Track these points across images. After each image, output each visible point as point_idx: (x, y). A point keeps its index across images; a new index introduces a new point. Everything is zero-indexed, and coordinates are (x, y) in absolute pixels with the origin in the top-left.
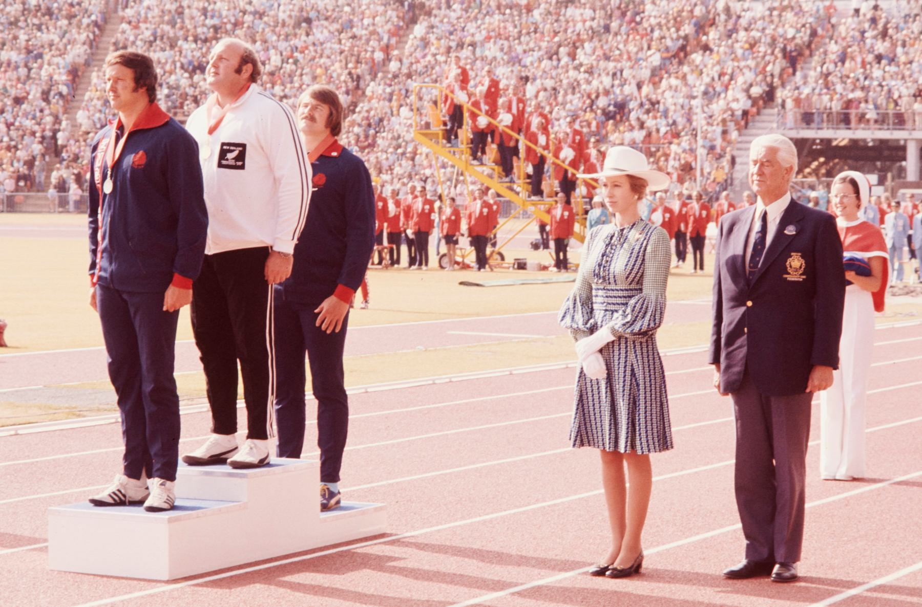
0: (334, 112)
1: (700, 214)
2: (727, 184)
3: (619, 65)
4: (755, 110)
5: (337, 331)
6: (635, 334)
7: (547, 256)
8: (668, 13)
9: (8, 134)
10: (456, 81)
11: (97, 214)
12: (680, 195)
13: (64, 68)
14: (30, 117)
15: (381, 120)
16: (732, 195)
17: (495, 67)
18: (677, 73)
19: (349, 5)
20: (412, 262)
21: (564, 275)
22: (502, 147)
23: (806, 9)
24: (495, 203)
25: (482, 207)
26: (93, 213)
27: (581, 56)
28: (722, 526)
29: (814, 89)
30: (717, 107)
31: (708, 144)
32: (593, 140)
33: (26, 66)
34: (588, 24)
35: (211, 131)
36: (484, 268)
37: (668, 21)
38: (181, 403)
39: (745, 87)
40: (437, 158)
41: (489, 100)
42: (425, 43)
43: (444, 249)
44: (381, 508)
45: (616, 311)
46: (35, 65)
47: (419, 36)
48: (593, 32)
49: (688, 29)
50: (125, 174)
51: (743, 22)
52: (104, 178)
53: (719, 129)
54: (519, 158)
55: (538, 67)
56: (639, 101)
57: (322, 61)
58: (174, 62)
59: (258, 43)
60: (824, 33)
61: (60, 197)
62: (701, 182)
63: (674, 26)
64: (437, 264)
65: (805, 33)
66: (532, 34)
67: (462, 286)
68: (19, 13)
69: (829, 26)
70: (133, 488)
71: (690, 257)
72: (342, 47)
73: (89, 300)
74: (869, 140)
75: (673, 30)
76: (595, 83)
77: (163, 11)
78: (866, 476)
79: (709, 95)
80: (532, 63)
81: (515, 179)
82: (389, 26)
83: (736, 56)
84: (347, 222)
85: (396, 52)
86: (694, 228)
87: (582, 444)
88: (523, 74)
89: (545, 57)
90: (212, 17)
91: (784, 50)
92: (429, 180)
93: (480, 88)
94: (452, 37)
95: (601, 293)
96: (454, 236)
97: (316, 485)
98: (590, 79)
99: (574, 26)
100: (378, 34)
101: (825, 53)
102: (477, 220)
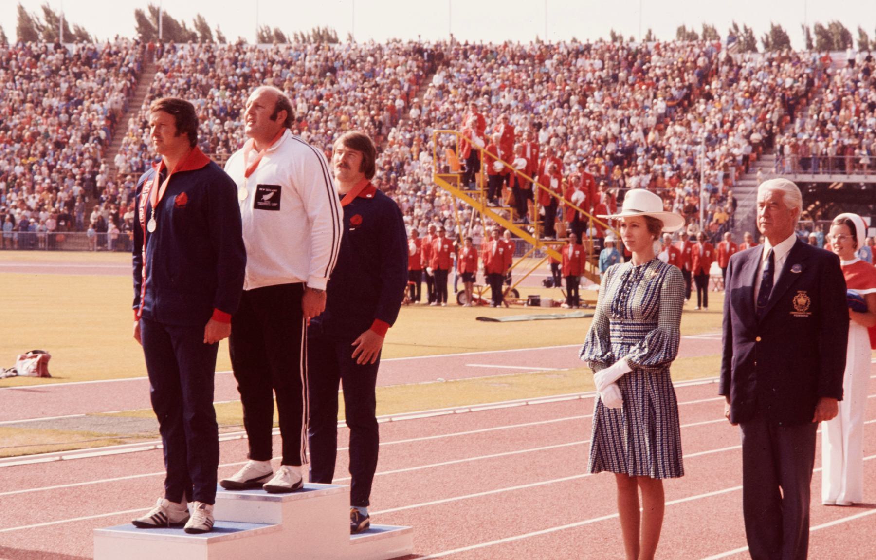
0: (367, 157)
1: (704, 254)
2: (729, 225)
3: (627, 113)
4: (755, 155)
5: (372, 363)
6: (652, 366)
7: (558, 294)
8: (672, 64)
9: (49, 176)
10: (473, 128)
11: (141, 251)
12: (685, 236)
13: (102, 114)
14: (70, 160)
15: (402, 164)
16: (733, 236)
17: (510, 114)
18: (681, 120)
19: (372, 55)
20: (431, 299)
21: (576, 312)
22: (516, 190)
23: (804, 60)
24: (510, 243)
25: (498, 247)
26: (137, 252)
27: (591, 105)
28: (729, 549)
29: (811, 136)
30: (719, 152)
31: (711, 187)
32: (602, 183)
33: (67, 112)
34: (597, 74)
35: (249, 173)
36: (500, 304)
37: (673, 72)
38: (220, 430)
39: (745, 133)
40: (455, 200)
41: (504, 145)
42: (443, 90)
43: (461, 287)
44: (408, 531)
45: (633, 345)
46: (75, 111)
47: (437, 85)
48: (602, 82)
49: (691, 78)
50: (167, 215)
51: (744, 72)
52: (148, 218)
53: (721, 174)
54: (533, 201)
55: (549, 115)
56: (645, 147)
57: (346, 108)
58: (207, 109)
59: (286, 91)
60: (821, 83)
61: (99, 236)
62: (704, 223)
63: (678, 76)
64: (455, 301)
65: (802, 82)
66: (545, 83)
67: (479, 322)
68: (60, 63)
69: (825, 76)
70: (174, 511)
71: (694, 295)
72: (366, 95)
73: (133, 332)
74: (862, 184)
75: (677, 80)
76: (604, 129)
77: (195, 61)
78: (863, 501)
79: (712, 142)
80: (544, 111)
81: (530, 221)
82: (410, 75)
83: (737, 105)
84: (379, 263)
85: (416, 100)
86: (698, 267)
87: (599, 470)
88: (536, 121)
89: (557, 104)
90: (242, 66)
91: (783, 97)
92: (448, 221)
93: (496, 134)
94: (469, 86)
95: (617, 327)
96: (472, 274)
97: (347, 509)
98: (599, 125)
99: (584, 76)
100: (399, 82)
101: (821, 102)
102: (493, 258)
